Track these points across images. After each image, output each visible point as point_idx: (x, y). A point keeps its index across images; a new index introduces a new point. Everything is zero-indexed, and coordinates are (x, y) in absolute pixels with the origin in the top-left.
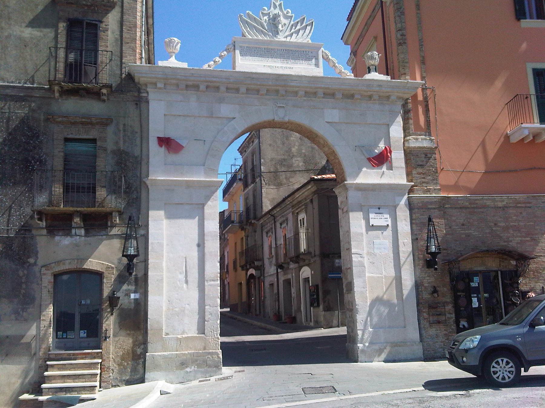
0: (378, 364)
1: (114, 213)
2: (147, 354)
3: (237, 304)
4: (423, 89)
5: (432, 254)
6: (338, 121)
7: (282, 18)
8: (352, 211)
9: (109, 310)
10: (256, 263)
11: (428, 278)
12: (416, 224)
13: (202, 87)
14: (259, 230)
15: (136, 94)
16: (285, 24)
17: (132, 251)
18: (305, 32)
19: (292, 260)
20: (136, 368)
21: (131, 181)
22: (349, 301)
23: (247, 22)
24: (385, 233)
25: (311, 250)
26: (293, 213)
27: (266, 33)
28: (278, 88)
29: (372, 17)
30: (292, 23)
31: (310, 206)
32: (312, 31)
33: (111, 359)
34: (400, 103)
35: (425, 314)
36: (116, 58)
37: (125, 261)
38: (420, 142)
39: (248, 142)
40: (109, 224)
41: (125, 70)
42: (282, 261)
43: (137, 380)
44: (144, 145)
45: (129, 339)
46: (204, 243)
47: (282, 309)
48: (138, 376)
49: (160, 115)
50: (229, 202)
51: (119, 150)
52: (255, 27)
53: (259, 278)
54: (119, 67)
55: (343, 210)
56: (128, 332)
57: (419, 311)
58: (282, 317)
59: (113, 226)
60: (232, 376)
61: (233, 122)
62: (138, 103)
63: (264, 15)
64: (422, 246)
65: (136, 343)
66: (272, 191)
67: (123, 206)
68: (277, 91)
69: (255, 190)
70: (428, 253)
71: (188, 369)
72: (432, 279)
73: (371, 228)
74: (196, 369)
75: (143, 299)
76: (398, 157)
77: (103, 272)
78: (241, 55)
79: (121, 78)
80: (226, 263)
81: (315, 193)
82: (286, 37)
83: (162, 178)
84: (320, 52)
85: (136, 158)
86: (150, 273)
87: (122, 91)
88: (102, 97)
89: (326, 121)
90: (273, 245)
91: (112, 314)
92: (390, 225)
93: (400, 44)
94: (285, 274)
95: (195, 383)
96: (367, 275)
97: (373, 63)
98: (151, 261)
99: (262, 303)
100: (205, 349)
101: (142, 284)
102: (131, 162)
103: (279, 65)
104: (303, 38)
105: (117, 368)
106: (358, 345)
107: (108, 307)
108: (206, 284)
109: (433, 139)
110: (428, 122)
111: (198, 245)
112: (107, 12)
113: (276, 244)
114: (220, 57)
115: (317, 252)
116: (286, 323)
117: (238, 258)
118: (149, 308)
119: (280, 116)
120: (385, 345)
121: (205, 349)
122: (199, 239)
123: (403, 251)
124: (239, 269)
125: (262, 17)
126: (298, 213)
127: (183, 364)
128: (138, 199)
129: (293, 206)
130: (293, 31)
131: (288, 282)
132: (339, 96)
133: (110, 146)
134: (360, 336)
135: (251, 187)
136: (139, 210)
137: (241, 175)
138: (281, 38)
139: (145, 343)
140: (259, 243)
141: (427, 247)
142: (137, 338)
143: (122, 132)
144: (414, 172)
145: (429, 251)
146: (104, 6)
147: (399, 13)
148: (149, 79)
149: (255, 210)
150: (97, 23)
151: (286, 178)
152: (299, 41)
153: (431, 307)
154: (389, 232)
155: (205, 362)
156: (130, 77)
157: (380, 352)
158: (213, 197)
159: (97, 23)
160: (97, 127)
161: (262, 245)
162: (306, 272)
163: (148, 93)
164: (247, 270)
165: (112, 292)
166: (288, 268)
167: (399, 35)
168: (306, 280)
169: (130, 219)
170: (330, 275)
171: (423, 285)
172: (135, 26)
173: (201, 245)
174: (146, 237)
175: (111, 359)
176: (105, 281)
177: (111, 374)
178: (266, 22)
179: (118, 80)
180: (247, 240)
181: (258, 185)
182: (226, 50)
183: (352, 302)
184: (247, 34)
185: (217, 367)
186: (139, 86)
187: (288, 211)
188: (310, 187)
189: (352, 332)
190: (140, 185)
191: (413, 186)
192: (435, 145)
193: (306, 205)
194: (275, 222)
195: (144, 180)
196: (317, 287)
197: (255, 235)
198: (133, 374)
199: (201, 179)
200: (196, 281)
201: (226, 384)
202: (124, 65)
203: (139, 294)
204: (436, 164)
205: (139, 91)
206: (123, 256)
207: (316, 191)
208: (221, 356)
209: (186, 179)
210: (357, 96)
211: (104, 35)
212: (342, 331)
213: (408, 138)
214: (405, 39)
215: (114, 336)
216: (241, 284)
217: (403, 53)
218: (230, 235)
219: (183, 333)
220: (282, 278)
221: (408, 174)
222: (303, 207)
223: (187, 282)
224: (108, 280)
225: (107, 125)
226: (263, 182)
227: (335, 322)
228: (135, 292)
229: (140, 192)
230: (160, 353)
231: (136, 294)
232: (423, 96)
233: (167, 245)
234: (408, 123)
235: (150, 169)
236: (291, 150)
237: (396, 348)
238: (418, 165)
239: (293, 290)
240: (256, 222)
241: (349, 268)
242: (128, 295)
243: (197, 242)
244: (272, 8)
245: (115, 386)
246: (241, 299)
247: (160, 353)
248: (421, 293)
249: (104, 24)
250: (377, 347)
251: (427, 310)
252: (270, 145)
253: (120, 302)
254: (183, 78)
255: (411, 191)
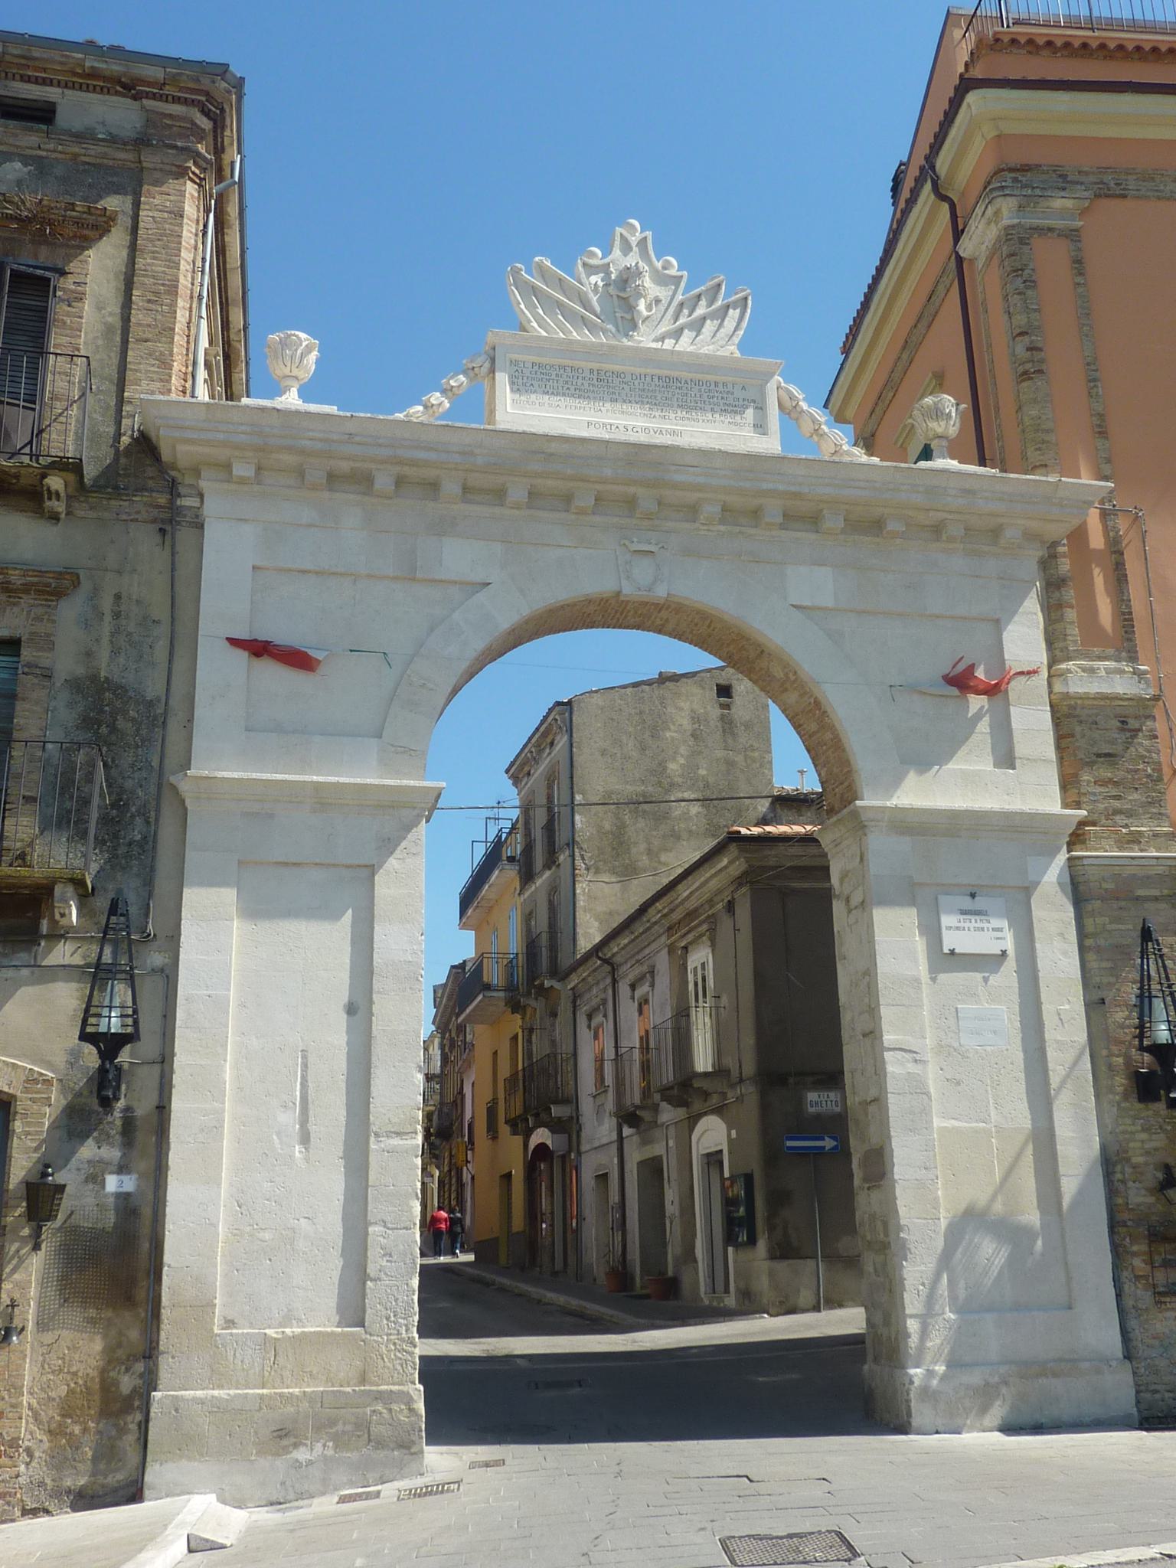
0: (983, 1441)
1: (58, 889)
2: (157, 1395)
3: (496, 1239)
4: (1104, 515)
5: (1157, 1050)
6: (830, 604)
7: (647, 282)
8: (885, 902)
9: (26, 1232)
10: (556, 1111)
11: (1144, 1136)
12: (1098, 950)
13: (383, 481)
14: (564, 1007)
15: (162, 500)
16: (658, 301)
17: (114, 1023)
18: (721, 325)
19: (666, 1093)
20: (113, 1447)
21: (129, 784)
22: (873, 1217)
23: (535, 291)
24: (994, 980)
25: (730, 1062)
26: (671, 949)
27: (595, 325)
28: (632, 490)
29: (925, 317)
30: (679, 297)
31: (726, 925)
32: (745, 324)
33: (25, 1412)
34: (1034, 554)
35: (1137, 1262)
36: (104, 386)
37: (91, 1057)
38: (1101, 679)
39: (538, 745)
40: (44, 926)
41: (131, 424)
42: (637, 1101)
43: (115, 1490)
44: (180, 665)
45: (92, 1340)
46: (371, 1002)
47: (635, 1254)
48: (120, 1476)
49: (236, 564)
50: (477, 929)
51: (94, 678)
52: (560, 305)
53: (564, 1158)
54: (112, 412)
55: (848, 900)
56: (92, 1312)
57: (1118, 1253)
58: (633, 1278)
59: (58, 935)
60: (458, 1482)
61: (482, 597)
62: (168, 528)
63: (591, 269)
64: (1122, 1026)
65: (120, 1353)
66: (607, 889)
67: (94, 867)
68: (631, 503)
69: (553, 889)
70: (1142, 1048)
71: (302, 1455)
72: (1159, 1141)
73: (947, 961)
74: (330, 1452)
75: (151, 1197)
76: (1033, 723)
77: (14, 1097)
78: (516, 388)
79: (117, 450)
80: (468, 1115)
81: (740, 881)
82: (662, 339)
83: (235, 775)
84: (771, 388)
85: (150, 704)
86: (177, 1104)
87: (116, 488)
88: (48, 503)
89: (791, 601)
90: (609, 1053)
91: (37, 1247)
92: (1011, 952)
93: (1025, 376)
94: (645, 1142)
95: (325, 1505)
96: (937, 1122)
97: (940, 430)
98: (182, 1060)
99: (572, 1238)
100: (363, 1380)
101: (147, 1138)
102: (133, 720)
103: (640, 423)
104: (718, 342)
105: (46, 1445)
106: (912, 1371)
107: (24, 1220)
108: (373, 1146)
109: (1146, 672)
110: (1125, 618)
111: (351, 1010)
112: (85, 243)
113: (616, 1047)
114: (444, 392)
115: (749, 1069)
116: (647, 1297)
117: (501, 1095)
118: (169, 1226)
119: (639, 581)
120: (1002, 1369)
121: (363, 1380)
122: (352, 987)
123: (1057, 1042)
124: (504, 1129)
125: (583, 275)
126: (685, 948)
127: (285, 1436)
128: (147, 846)
129: (670, 928)
130: (682, 321)
131: (653, 1170)
132: (833, 522)
133: (65, 664)
134: (913, 1341)
135: (542, 880)
136: (148, 882)
137: (516, 847)
138: (644, 339)
139: (150, 1353)
140: (565, 1048)
141: (1142, 1029)
142: (120, 1333)
143: (108, 618)
144: (1086, 777)
145: (1146, 1043)
146: (77, 223)
147: (1019, 282)
148: (207, 450)
149: (553, 948)
150: (48, 274)
151: (649, 852)
152: (705, 350)
153: (1156, 1237)
154: (1007, 977)
155: (362, 1426)
156: (145, 445)
157: (985, 1395)
158: (403, 844)
159: (48, 274)
160: (26, 600)
161: (575, 1055)
162: (712, 1134)
163: (201, 496)
164: (528, 1134)
165: (40, 1167)
166: (655, 1124)
167: (1020, 349)
168: (713, 1159)
169: (113, 909)
170: (789, 1143)
171: (1128, 1160)
172: (173, 290)
173: (359, 1009)
174: (168, 976)
175: (25, 1412)
176: (18, 1126)
177: (22, 1468)
178: (596, 289)
179: (106, 454)
180: (530, 1041)
181: (565, 870)
182: (465, 373)
183: (887, 1219)
184: (535, 324)
185: (406, 1446)
186: (173, 473)
187: (653, 946)
188: (725, 861)
189: (887, 1323)
190: (158, 798)
191: (1082, 824)
192: (1152, 691)
193: (713, 920)
194: (614, 981)
195: (173, 779)
196: (749, 1179)
197: (553, 1025)
198: (102, 1466)
199: (368, 781)
200: (340, 1133)
201: (434, 1513)
202: (127, 408)
203: (134, 1177)
204: (1158, 753)
205: (173, 488)
206: (84, 1037)
207: (745, 874)
208: (420, 1406)
209: (315, 778)
210: (892, 526)
211: (68, 314)
212: (846, 1320)
213: (1063, 666)
214: (1042, 361)
215: (42, 1326)
216: (508, 1176)
217: (1035, 401)
218: (480, 1028)
219: (287, 1320)
220: (635, 1155)
221: (1067, 784)
222: (705, 927)
223: (305, 1139)
224: (29, 1124)
225: (59, 594)
226: (579, 862)
227: (806, 1296)
228: (122, 1169)
229: (157, 820)
230: (199, 1393)
231: (125, 1178)
232: (1106, 530)
233: (242, 1005)
234: (1061, 619)
235: (197, 742)
236: (665, 769)
237: (1043, 1381)
238: (1099, 756)
239: (671, 1195)
240: (557, 985)
241: (875, 1100)
242: (95, 1179)
243: (345, 998)
244: (617, 252)
245: (34, 1512)
246: (509, 1226)
247: (199, 1393)
248: (1121, 1187)
249: (71, 279)
250: (975, 1378)
251: (1144, 1248)
252: (603, 752)
253: (67, 1203)
254: (319, 445)
255: (1076, 838)
